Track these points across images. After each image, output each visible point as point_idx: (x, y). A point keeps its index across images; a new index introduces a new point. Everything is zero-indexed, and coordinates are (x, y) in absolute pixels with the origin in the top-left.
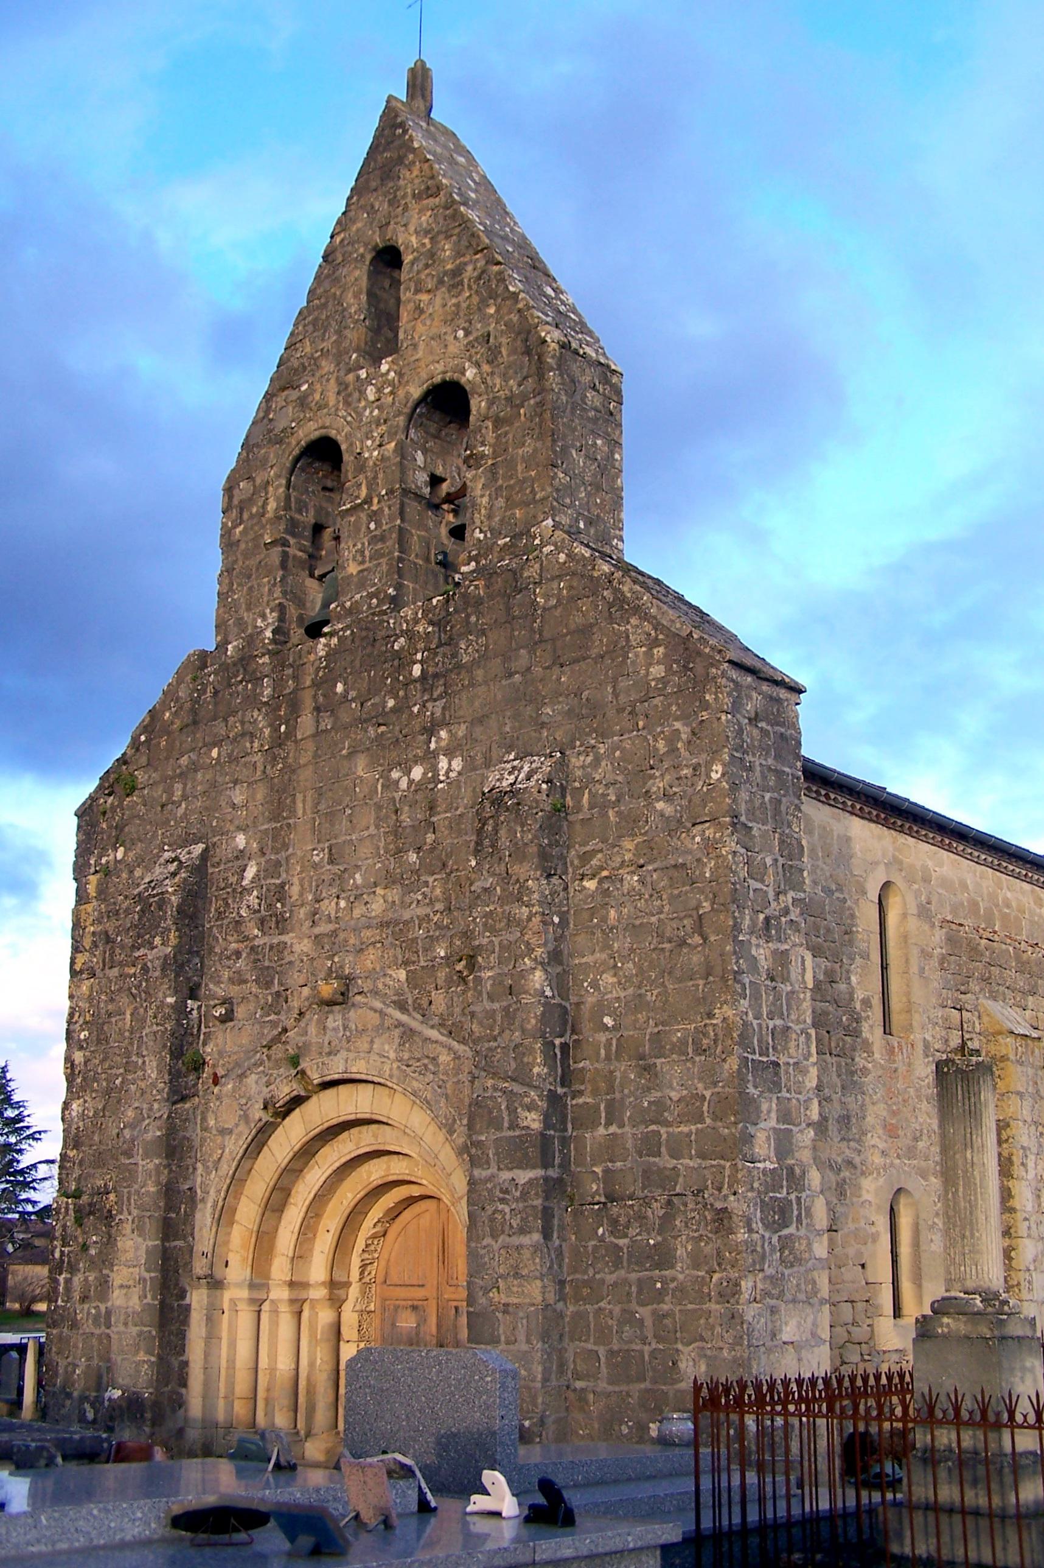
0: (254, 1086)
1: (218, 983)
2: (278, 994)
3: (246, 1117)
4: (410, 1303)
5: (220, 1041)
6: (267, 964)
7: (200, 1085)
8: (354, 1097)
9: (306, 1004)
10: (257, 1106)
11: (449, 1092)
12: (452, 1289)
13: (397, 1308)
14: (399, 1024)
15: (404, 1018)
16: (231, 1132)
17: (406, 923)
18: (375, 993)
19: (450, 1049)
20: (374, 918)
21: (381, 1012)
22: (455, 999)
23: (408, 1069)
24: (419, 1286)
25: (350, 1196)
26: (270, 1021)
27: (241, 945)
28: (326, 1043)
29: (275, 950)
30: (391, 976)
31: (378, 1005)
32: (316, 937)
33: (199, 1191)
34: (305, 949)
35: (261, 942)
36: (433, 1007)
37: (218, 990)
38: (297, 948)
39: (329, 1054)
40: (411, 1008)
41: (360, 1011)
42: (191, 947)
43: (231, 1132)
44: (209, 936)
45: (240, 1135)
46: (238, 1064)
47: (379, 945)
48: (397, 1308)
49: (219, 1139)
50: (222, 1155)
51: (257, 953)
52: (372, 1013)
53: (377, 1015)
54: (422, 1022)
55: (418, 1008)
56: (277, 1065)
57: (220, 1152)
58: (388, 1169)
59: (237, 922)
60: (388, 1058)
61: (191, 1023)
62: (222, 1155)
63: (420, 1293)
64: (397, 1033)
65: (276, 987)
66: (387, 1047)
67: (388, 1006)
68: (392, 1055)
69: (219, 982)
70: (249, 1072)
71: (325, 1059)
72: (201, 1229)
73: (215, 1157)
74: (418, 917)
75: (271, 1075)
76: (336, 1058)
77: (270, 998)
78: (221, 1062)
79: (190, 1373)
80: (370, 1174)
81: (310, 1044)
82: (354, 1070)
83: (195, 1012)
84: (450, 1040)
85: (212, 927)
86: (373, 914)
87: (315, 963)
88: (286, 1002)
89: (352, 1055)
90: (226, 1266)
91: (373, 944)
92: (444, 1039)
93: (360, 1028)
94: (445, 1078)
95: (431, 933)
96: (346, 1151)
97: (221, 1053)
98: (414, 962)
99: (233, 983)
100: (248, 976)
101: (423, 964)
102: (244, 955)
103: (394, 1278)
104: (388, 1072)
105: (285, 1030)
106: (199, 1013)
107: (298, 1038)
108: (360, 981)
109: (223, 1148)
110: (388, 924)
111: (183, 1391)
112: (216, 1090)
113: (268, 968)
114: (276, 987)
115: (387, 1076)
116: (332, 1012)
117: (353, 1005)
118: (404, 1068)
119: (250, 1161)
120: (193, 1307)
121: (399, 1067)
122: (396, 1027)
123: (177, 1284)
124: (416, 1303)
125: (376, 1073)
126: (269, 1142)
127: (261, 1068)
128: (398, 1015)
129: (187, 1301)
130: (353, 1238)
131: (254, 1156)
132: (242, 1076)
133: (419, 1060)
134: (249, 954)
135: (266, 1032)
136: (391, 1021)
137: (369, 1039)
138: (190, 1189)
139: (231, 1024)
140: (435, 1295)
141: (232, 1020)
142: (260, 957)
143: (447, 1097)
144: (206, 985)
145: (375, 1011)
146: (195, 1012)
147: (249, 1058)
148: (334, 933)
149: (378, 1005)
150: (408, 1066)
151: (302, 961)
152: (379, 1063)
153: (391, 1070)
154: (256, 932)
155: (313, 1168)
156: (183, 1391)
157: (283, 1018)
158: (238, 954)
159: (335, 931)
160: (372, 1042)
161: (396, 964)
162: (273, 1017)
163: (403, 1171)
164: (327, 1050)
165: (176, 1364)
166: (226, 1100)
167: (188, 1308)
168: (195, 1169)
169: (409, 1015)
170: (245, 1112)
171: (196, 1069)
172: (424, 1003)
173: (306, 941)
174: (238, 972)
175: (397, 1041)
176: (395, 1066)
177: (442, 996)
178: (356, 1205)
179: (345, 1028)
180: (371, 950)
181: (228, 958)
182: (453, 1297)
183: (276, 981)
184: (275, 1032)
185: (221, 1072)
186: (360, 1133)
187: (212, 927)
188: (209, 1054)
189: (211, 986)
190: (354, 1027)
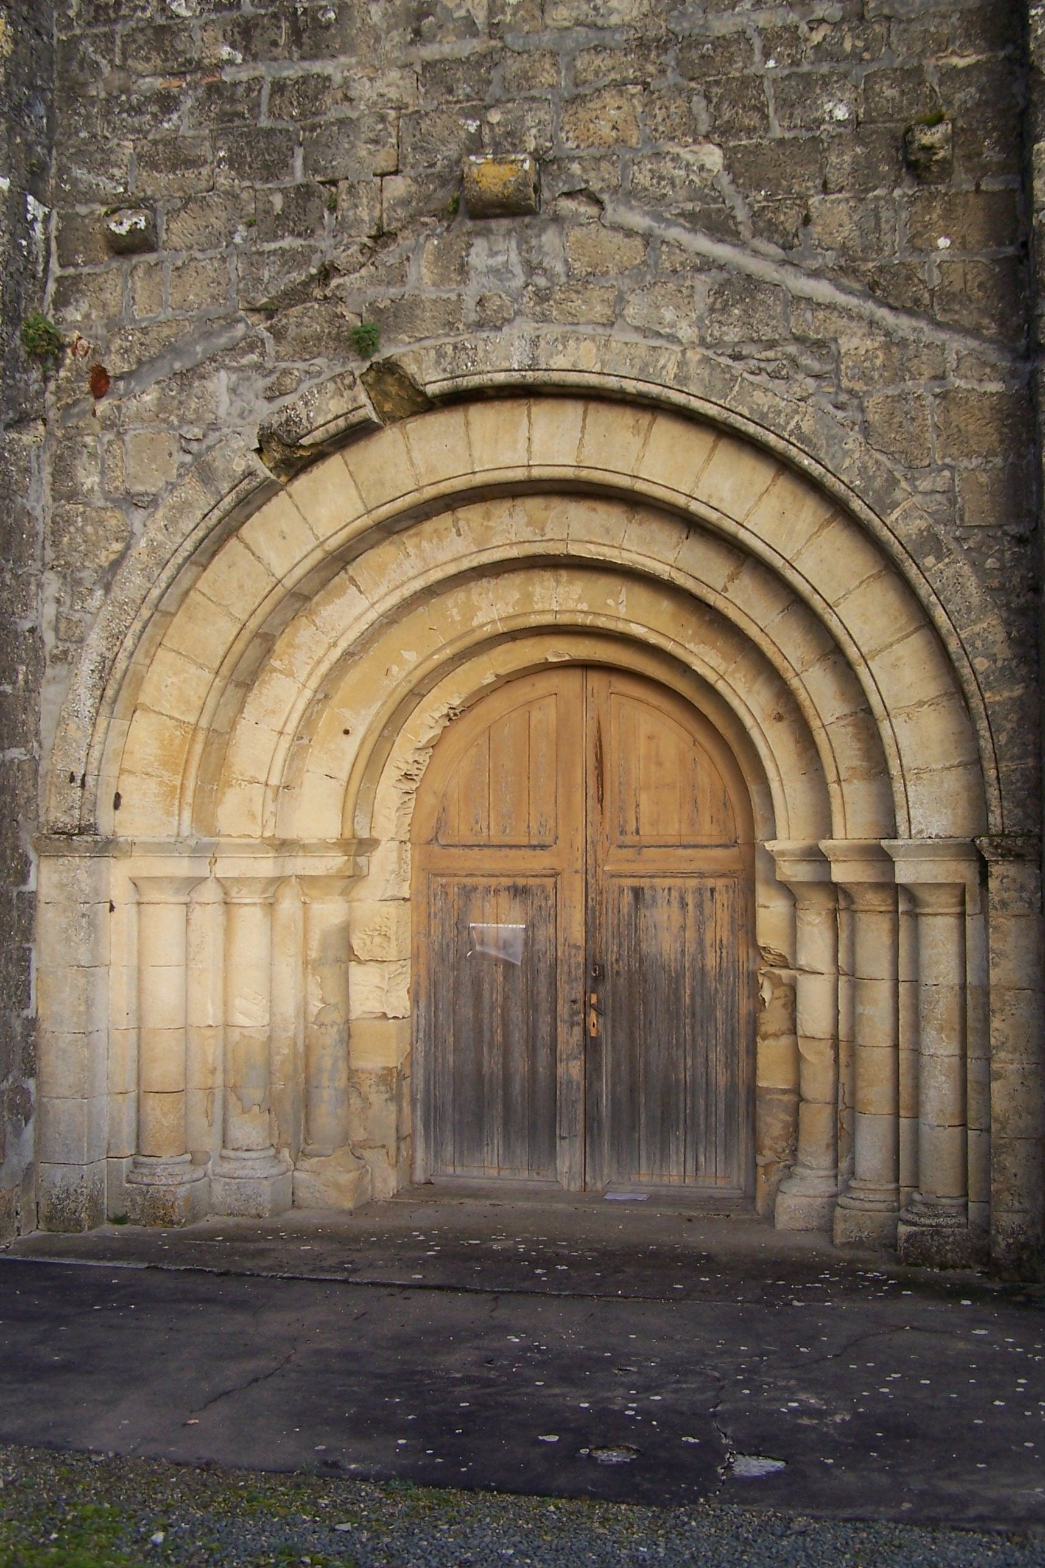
0: (225, 398)
1: (105, 165)
2: (305, 192)
3: (205, 474)
4: (506, 882)
5: (112, 296)
6: (264, 122)
7: (50, 398)
8: (523, 432)
9: (400, 213)
10: (238, 443)
11: (873, 417)
12: (628, 853)
13: (467, 892)
14: (706, 264)
15: (723, 251)
16: (154, 502)
17: (720, 43)
18: (630, 195)
19: (872, 323)
20: (617, 28)
21: (647, 238)
22: (885, 215)
23: (738, 367)
24: (534, 847)
25: (411, 657)
26: (283, 252)
27: (175, 82)
28: (470, 302)
29: (291, 94)
30: (676, 158)
31: (639, 221)
32: (427, 65)
33: (49, 638)
34: (393, 93)
35: (244, 76)
36: (816, 230)
37: (103, 181)
38: (365, 90)
39: (480, 325)
40: (745, 232)
41: (576, 233)
42: (32, 75)
43: (154, 502)
44: (68, 59)
45: (183, 509)
46: (171, 349)
47: (633, 89)
48: (467, 892)
49: (113, 520)
50: (123, 555)
51: (232, 100)
52: (619, 238)
53: (638, 242)
54: (783, 263)
55: (768, 229)
56: (306, 348)
57: (118, 546)
58: (528, 597)
59: (161, 30)
60: (673, 339)
61: (34, 249)
62: (123, 555)
63: (541, 861)
64: (703, 283)
65: (298, 174)
66: (669, 315)
67: (669, 223)
68: (687, 332)
69: (106, 163)
70: (209, 367)
71: (467, 339)
72: (60, 722)
73: (104, 558)
74: (760, 31)
75: (286, 372)
76: (498, 338)
77: (278, 201)
78: (117, 343)
79: (43, 1044)
80: (470, 611)
81: (416, 302)
82: (559, 362)
83: (39, 227)
84: (870, 305)
85: (74, 41)
86: (614, 20)
87: (425, 125)
88: (333, 209)
89: (550, 331)
90: (116, 806)
91: (619, 86)
92: (853, 302)
93: (579, 268)
94: (859, 386)
95: (805, 68)
96: (443, 557)
97: (114, 325)
98: (750, 131)
99: (154, 166)
100: (206, 150)
101: (777, 132)
102: (188, 103)
103: (461, 828)
104: (672, 370)
105: (327, 273)
106: (46, 228)
107: (371, 292)
108: (575, 168)
109: (128, 540)
110: (662, 45)
111: (31, 1084)
112: (103, 406)
113: (269, 133)
114: (298, 174)
115: (669, 378)
116: (486, 233)
117: (557, 219)
118: (725, 361)
119: (195, 569)
120: (42, 898)
121: (706, 360)
122: (699, 270)
123: (16, 848)
124: (521, 882)
125: (634, 373)
126: (245, 531)
127: (254, 357)
128: (702, 244)
129: (31, 886)
130: (389, 746)
131: (203, 560)
132: (185, 378)
133: (771, 344)
134: (200, 104)
135: (266, 275)
136: (679, 257)
137: (611, 296)
138: (32, 630)
139: (151, 258)
140: (579, 865)
141: (151, 248)
142: (242, 108)
143: (866, 429)
144: (62, 170)
145: (629, 233)
146: (39, 227)
147: (207, 335)
148: (487, 60)
149: (639, 221)
150: (737, 357)
151: (383, 119)
152: (642, 351)
153: (681, 365)
154: (225, 52)
155: (341, 591)
156: (31, 1084)
157: (323, 245)
158: (167, 102)
159: (491, 53)
160: (621, 300)
161: (695, 133)
162: (288, 242)
163: (571, 605)
164: (473, 317)
165: (17, 1026)
166: (134, 432)
167: (30, 902)
168: (40, 586)
169: (742, 245)
170: (197, 456)
171: (42, 358)
172: (789, 219)
173: (394, 75)
174: (172, 142)
175: (702, 302)
176: (693, 356)
177: (843, 206)
178: (424, 678)
179: (531, 269)
180: (610, 98)
181: (137, 110)
182: (626, 868)
183: (298, 163)
184: (297, 277)
185: (114, 364)
186: (488, 516)
187: (74, 41)
188: (75, 326)
189: (79, 172)
190: (559, 268)
